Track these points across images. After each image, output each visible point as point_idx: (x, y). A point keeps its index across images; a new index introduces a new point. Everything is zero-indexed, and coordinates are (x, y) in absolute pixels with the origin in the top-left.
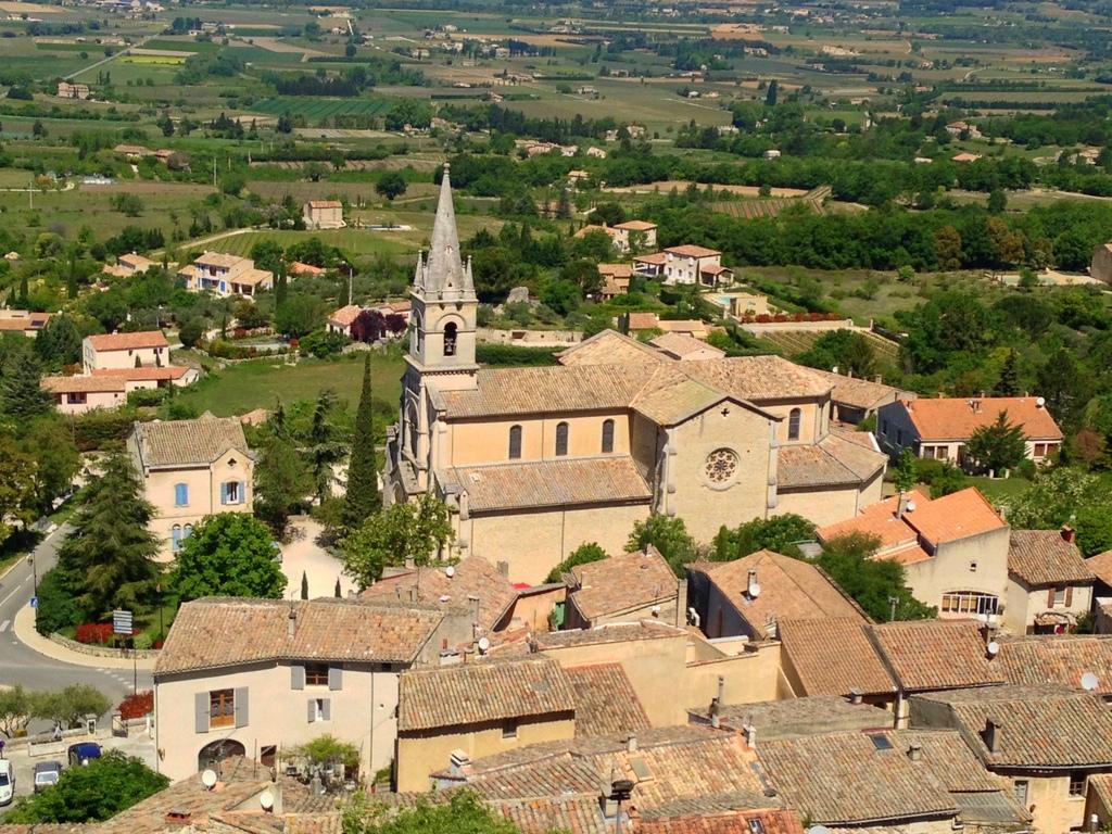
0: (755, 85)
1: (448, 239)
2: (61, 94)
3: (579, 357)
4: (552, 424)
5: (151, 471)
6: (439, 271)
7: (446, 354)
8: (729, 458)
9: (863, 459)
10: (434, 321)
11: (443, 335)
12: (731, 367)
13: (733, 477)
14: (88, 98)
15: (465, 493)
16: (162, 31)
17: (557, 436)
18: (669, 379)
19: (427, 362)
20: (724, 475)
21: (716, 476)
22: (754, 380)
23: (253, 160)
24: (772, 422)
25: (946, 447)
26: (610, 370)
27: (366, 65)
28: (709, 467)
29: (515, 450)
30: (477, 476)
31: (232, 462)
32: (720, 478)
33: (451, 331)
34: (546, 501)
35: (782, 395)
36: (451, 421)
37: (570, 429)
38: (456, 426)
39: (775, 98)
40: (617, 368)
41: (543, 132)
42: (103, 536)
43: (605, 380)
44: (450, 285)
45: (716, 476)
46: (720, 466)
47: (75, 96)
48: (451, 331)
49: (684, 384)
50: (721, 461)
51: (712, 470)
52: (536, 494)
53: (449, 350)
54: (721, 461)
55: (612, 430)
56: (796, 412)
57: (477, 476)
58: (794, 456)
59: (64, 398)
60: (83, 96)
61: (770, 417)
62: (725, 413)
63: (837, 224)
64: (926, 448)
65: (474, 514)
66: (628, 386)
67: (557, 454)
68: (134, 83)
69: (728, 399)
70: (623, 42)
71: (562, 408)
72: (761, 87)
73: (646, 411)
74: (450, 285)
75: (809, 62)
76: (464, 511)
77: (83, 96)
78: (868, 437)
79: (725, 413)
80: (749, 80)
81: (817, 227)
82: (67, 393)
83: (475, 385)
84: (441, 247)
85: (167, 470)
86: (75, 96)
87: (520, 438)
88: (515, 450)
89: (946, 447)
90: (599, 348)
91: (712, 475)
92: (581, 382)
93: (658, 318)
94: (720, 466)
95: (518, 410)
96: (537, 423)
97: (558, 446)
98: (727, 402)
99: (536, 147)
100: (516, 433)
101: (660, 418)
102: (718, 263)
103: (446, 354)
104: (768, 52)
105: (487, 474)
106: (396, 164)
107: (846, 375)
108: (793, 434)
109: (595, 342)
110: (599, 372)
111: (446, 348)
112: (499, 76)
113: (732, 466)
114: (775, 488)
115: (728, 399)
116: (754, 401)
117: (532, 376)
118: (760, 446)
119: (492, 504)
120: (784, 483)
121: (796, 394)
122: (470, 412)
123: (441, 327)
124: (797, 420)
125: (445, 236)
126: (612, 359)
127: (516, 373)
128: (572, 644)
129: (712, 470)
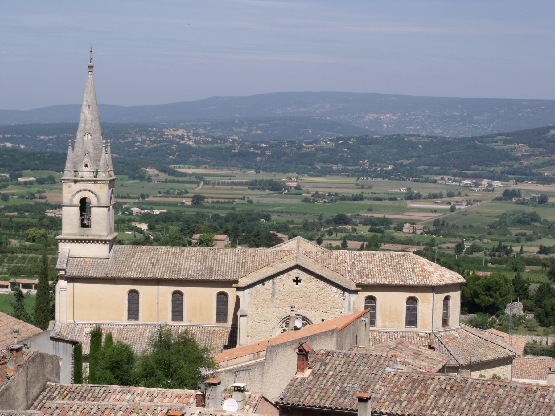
1: (87, 127)
2: (405, 230)
4: (170, 290)
6: (80, 153)
10: (70, 196)
14: (422, 234)
16: (494, 198)
24: (347, 294)
33: (84, 206)
36: (72, 279)
37: (185, 298)
44: (86, 166)
47: (414, 233)
48: (84, 206)
55: (227, 302)
60: (418, 232)
68: (468, 227)
69: (298, 267)
74: (86, 166)
77: (418, 232)
84: (82, 134)
86: (414, 233)
87: (138, 302)
95: (134, 275)
97: (173, 312)
100: (133, 297)
115: (298, 267)
124: (415, 309)
125: (85, 124)
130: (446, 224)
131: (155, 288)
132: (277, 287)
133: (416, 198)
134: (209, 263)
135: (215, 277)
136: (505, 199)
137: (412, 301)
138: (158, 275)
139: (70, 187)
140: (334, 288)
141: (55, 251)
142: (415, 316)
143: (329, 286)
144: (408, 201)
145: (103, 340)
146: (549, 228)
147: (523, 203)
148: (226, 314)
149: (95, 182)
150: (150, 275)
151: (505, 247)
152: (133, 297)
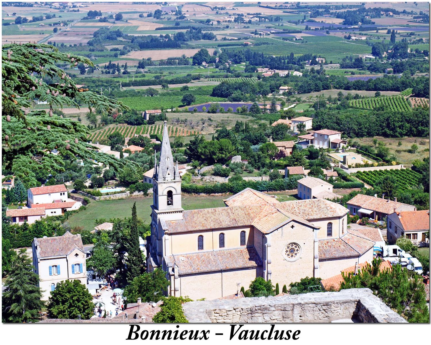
0: (386, 31)
3: (234, 201)
4: (217, 234)
5: (41, 260)
7: (168, 204)
8: (296, 247)
9: (362, 244)
11: (166, 197)
12: (300, 205)
13: (297, 257)
15: (176, 266)
17: (220, 239)
18: (270, 211)
19: (159, 209)
20: (294, 255)
21: (290, 255)
22: (310, 210)
23: (123, 86)
25: (417, 234)
26: (243, 208)
27: (184, 31)
28: (287, 251)
29: (201, 246)
30: (183, 258)
31: (77, 255)
32: (292, 256)
33: (170, 194)
34: (214, 269)
35: (323, 216)
37: (225, 236)
38: (173, 236)
39: (394, 40)
40: (247, 207)
41: (273, 64)
42: (16, 290)
43: (241, 213)
45: (290, 255)
46: (292, 251)
48: (170, 194)
49: (276, 214)
50: (293, 249)
51: (288, 253)
52: (209, 266)
53: (170, 203)
54: (293, 249)
56: (330, 224)
57: (183, 258)
58: (329, 244)
59: (17, 219)
61: (314, 228)
62: (292, 227)
63: (399, 116)
64: (407, 234)
65: (180, 276)
66: (252, 215)
67: (220, 247)
69: (294, 221)
70: (318, 12)
71: (221, 227)
72: (388, 33)
73: (258, 227)
75: (415, 18)
76: (176, 274)
78: (377, 231)
79: (292, 227)
80: (382, 29)
81: (389, 117)
82: (19, 217)
83: (182, 218)
85: (51, 259)
88: (201, 246)
89: (417, 234)
90: (243, 197)
91: (288, 255)
92: (231, 214)
93: (304, 169)
94: (292, 251)
95: (201, 228)
96: (210, 233)
98: (292, 222)
99: (267, 72)
100: (201, 239)
101: (264, 231)
102: (339, 137)
103: (168, 204)
104: (394, 13)
105: (187, 258)
106: (193, 85)
107: (382, 198)
108: (330, 234)
109: (242, 194)
110: (239, 210)
111: (168, 202)
112: (252, 33)
113: (297, 250)
114: (318, 259)
115: (294, 221)
116: (310, 221)
117: (208, 212)
118: (310, 240)
119: (190, 271)
120: (323, 257)
121: (330, 216)
122: (179, 230)
123: (166, 193)
124: (331, 228)
126: (247, 203)
127: (201, 211)
128: (403, 314)
129: (288, 253)
130: (56, 45)
131: (211, 233)
132: (283, 231)
133: (23, 22)
134: (232, 216)
135: (240, 225)
136: (90, 18)
137: (330, 224)
138: (213, 227)
139: (162, 186)
140: (309, 228)
141: (156, 217)
142: (331, 231)
143: (307, 227)
144: (19, 25)
145: (143, 248)
146: (132, 42)
147: (104, 20)
148: (245, 241)
149: (175, 182)
150: (209, 227)
151: (114, 65)
152: (201, 239)
